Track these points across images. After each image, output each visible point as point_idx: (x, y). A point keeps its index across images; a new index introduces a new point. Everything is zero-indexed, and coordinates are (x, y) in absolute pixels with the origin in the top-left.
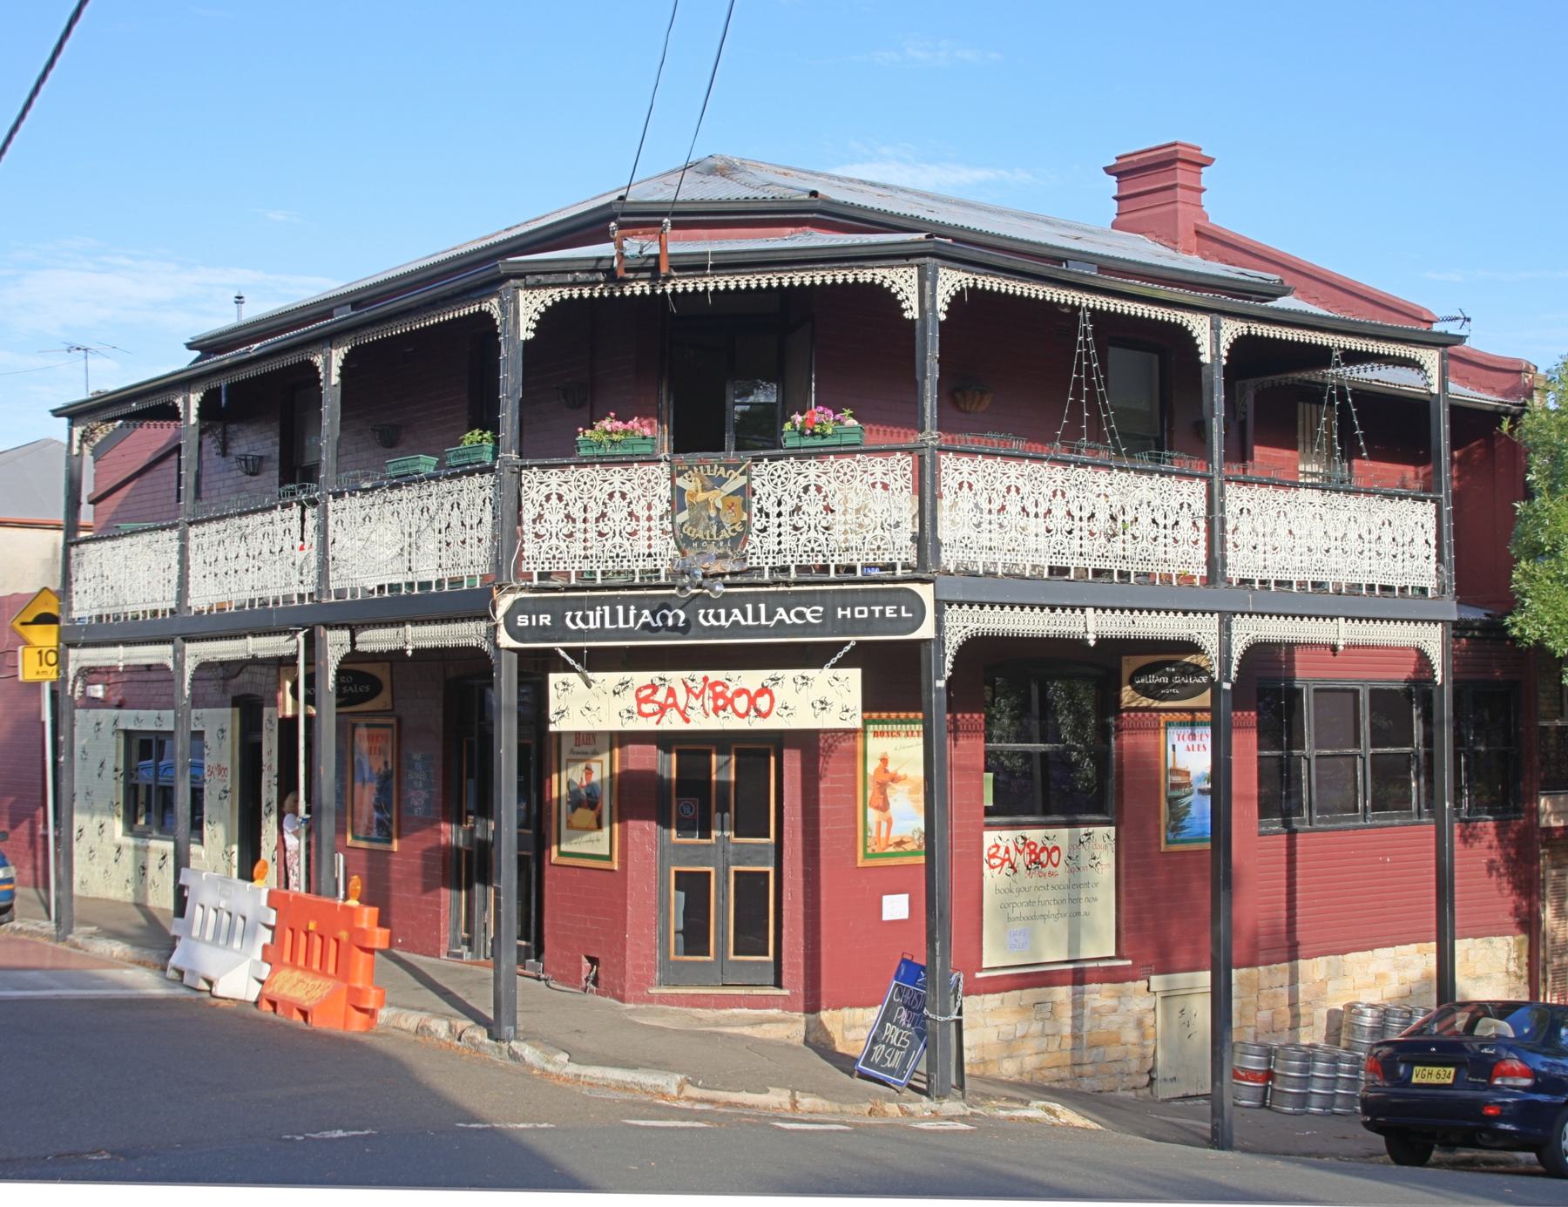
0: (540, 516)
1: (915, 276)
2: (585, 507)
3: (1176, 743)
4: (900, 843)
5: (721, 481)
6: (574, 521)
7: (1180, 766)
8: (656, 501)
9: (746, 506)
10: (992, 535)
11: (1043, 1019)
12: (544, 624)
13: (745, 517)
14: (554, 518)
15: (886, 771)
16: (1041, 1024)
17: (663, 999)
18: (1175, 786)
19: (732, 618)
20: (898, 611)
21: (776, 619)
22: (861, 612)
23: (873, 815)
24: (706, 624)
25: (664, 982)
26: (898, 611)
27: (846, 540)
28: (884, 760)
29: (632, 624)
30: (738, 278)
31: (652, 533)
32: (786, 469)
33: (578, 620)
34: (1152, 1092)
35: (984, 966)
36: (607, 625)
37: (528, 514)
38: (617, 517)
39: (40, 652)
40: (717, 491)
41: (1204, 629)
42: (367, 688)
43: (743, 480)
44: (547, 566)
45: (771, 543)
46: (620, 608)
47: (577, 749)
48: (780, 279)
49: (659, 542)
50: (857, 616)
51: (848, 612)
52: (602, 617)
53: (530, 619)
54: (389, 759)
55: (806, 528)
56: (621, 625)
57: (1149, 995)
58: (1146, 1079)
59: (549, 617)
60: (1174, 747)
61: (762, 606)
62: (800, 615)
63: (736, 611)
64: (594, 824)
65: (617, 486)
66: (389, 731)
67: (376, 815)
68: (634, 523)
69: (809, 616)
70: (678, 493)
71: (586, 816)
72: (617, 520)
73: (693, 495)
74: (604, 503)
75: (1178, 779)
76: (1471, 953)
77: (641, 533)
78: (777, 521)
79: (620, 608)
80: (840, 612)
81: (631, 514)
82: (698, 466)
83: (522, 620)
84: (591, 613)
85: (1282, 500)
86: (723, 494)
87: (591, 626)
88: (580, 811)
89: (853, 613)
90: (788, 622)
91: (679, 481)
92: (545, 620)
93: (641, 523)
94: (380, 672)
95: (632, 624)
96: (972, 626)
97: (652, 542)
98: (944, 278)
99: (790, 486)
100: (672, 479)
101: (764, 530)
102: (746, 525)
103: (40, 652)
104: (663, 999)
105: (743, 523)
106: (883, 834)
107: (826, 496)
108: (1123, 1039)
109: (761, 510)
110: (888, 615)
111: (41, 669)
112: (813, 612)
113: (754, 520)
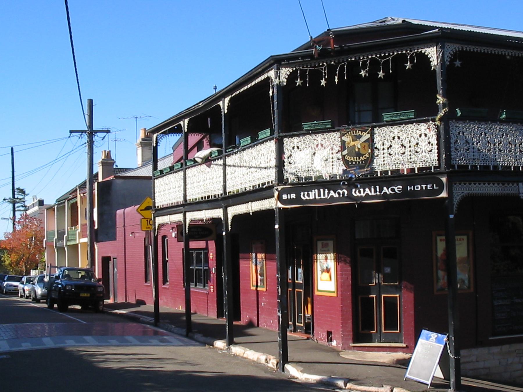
5: (360, 137)
6: (405, 147)
12: (293, 198)
14: (397, 146)
19: (366, 193)
20: (433, 187)
22: (417, 188)
26: (433, 187)
29: (326, 196)
32: (412, 128)
33: (306, 196)
35: (181, 309)
37: (452, 141)
39: (147, 220)
40: (359, 141)
47: (323, 249)
50: (416, 189)
51: (412, 188)
52: (315, 194)
53: (287, 196)
56: (322, 197)
61: (378, 187)
62: (393, 190)
63: (367, 190)
64: (329, 279)
65: (396, 134)
69: (396, 190)
70: (343, 143)
71: (326, 275)
73: (349, 143)
78: (382, 152)
80: (409, 188)
81: (429, 143)
82: (350, 131)
83: (285, 197)
84: (310, 193)
86: (361, 142)
88: (324, 273)
90: (388, 193)
91: (343, 138)
92: (293, 196)
94: (43, 229)
95: (326, 196)
96: (466, 192)
100: (341, 137)
103: (147, 220)
107: (402, 141)
110: (428, 188)
111: (148, 227)
112: (398, 188)
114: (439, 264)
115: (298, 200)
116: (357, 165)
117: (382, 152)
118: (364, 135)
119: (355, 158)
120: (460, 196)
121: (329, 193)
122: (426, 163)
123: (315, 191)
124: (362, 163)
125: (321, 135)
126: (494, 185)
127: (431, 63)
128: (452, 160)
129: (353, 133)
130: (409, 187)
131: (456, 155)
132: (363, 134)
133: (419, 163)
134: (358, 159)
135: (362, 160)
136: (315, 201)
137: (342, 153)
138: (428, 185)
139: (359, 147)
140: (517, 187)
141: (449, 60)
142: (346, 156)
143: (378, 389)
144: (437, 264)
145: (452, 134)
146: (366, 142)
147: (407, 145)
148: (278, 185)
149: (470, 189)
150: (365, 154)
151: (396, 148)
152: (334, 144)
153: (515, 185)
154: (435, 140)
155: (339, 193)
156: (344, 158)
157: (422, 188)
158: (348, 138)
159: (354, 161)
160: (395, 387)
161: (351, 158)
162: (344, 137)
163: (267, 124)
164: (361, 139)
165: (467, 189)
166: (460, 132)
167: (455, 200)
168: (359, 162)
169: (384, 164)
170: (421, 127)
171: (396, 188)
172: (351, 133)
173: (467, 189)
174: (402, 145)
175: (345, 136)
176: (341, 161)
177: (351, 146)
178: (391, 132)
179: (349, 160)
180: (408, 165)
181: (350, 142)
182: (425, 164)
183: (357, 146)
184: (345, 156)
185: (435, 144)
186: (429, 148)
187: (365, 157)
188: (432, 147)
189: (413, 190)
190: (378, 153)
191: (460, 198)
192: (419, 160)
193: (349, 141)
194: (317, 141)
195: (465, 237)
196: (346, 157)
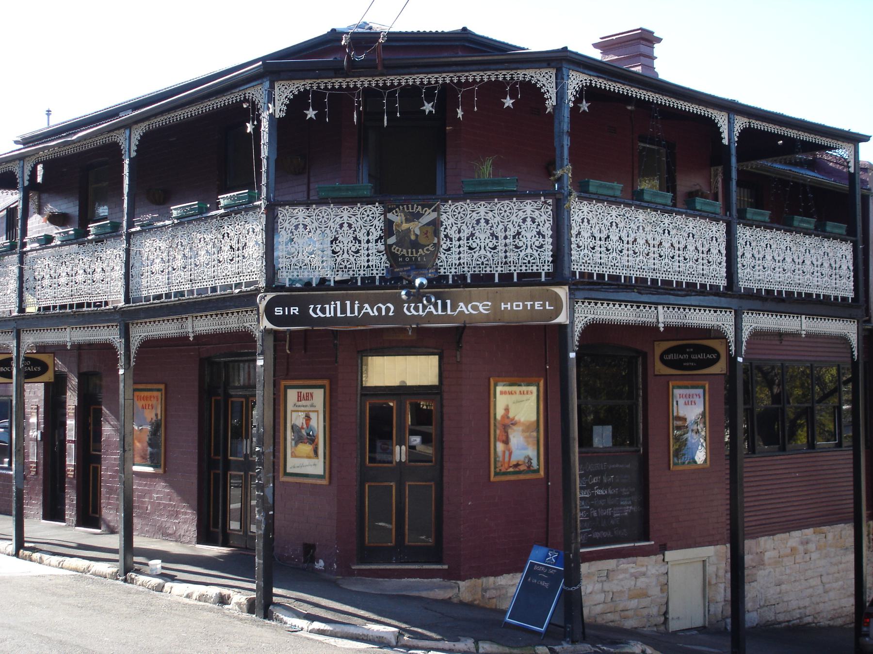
0: (519, 233)
1: (554, 76)
2: (368, 232)
3: (679, 400)
4: (517, 465)
5: (419, 216)
7: (681, 414)
8: (373, 230)
9: (436, 233)
10: (602, 255)
11: (602, 582)
13: (436, 241)
15: (508, 418)
16: (601, 584)
17: (362, 573)
18: (678, 428)
20: (544, 305)
21: (458, 310)
22: (518, 306)
23: (500, 447)
24: (315, 316)
25: (362, 561)
26: (544, 305)
27: (506, 257)
28: (507, 410)
29: (356, 314)
30: (444, 75)
31: (461, 249)
33: (412, 309)
34: (666, 629)
36: (339, 315)
38: (529, 235)
40: (416, 223)
41: (724, 321)
42: (39, 369)
43: (434, 215)
44: (524, 268)
45: (454, 259)
46: (348, 303)
47: (300, 403)
48: (459, 77)
49: (374, 257)
50: (515, 308)
51: (509, 306)
52: (335, 309)
54: (159, 413)
55: (478, 248)
56: (349, 314)
57: (664, 563)
58: (663, 619)
59: (297, 308)
60: (677, 402)
64: (312, 454)
66: (159, 394)
67: (149, 449)
68: (541, 239)
69: (481, 308)
70: (389, 224)
71: (306, 448)
72: (529, 237)
73: (399, 225)
74: (519, 225)
75: (679, 423)
76: (843, 532)
77: (362, 252)
79: (348, 303)
80: (503, 306)
82: (403, 205)
83: (278, 311)
84: (327, 306)
85: (768, 237)
86: (420, 225)
87: (328, 315)
89: (512, 306)
90: (467, 312)
91: (390, 216)
92: (295, 310)
93: (363, 245)
96: (590, 316)
97: (508, 254)
98: (572, 79)
99: (467, 219)
100: (385, 214)
101: (449, 249)
102: (437, 246)
104: (362, 573)
105: (435, 244)
106: (507, 459)
108: (650, 593)
109: (446, 236)
110: (536, 308)
113: (442, 243)
114: (498, 432)
115: (303, 318)
116: (412, 263)
117: (457, 243)
118: (427, 213)
119: (410, 250)
120: (582, 322)
121: (360, 309)
122: (532, 266)
123: (336, 304)
124: (422, 259)
125: (305, 210)
126: (602, 305)
127: (547, 102)
128: (572, 264)
129: (408, 209)
130: (502, 304)
131: (469, 259)
132: (426, 211)
133: (474, 267)
134: (414, 253)
135: (421, 255)
136: (334, 320)
137: (385, 241)
138: (536, 303)
139: (418, 232)
140: (656, 311)
141: (573, 99)
142: (394, 246)
143: (454, 645)
144: (495, 431)
145: (573, 220)
146: (429, 225)
147: (501, 235)
148: (266, 291)
149: (596, 313)
150: (428, 245)
151: (482, 237)
152: (510, 221)
153: (653, 309)
154: (549, 229)
155: (379, 309)
156: (390, 249)
157: (525, 306)
158: (398, 216)
159: (408, 257)
160: (481, 640)
161: (402, 251)
162: (391, 213)
163: (248, 180)
164: (420, 220)
165: (592, 313)
166: (527, 217)
167: (576, 329)
168: (416, 258)
169: (368, 267)
170: (525, 206)
171: (481, 305)
172: (403, 208)
173: (592, 313)
174: (355, 238)
175: (393, 213)
176: (383, 255)
177: (402, 231)
178: (337, 216)
179: (399, 253)
180: (502, 267)
181: (402, 222)
182: (531, 268)
183: (414, 231)
184: (391, 246)
185: (549, 236)
186: (492, 243)
187: (428, 250)
188: (360, 246)
189: (509, 309)
190: (358, 247)
191: (583, 326)
192: (474, 261)
193: (400, 222)
194: (341, 218)
195: (534, 389)
196: (393, 248)
